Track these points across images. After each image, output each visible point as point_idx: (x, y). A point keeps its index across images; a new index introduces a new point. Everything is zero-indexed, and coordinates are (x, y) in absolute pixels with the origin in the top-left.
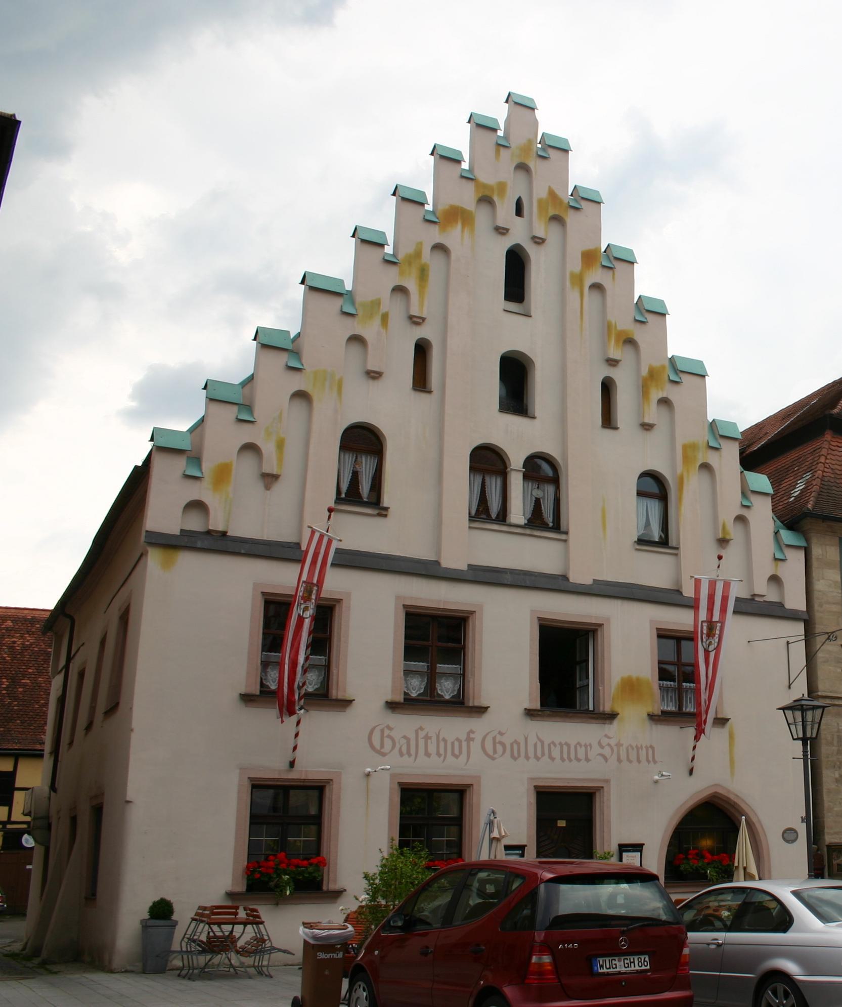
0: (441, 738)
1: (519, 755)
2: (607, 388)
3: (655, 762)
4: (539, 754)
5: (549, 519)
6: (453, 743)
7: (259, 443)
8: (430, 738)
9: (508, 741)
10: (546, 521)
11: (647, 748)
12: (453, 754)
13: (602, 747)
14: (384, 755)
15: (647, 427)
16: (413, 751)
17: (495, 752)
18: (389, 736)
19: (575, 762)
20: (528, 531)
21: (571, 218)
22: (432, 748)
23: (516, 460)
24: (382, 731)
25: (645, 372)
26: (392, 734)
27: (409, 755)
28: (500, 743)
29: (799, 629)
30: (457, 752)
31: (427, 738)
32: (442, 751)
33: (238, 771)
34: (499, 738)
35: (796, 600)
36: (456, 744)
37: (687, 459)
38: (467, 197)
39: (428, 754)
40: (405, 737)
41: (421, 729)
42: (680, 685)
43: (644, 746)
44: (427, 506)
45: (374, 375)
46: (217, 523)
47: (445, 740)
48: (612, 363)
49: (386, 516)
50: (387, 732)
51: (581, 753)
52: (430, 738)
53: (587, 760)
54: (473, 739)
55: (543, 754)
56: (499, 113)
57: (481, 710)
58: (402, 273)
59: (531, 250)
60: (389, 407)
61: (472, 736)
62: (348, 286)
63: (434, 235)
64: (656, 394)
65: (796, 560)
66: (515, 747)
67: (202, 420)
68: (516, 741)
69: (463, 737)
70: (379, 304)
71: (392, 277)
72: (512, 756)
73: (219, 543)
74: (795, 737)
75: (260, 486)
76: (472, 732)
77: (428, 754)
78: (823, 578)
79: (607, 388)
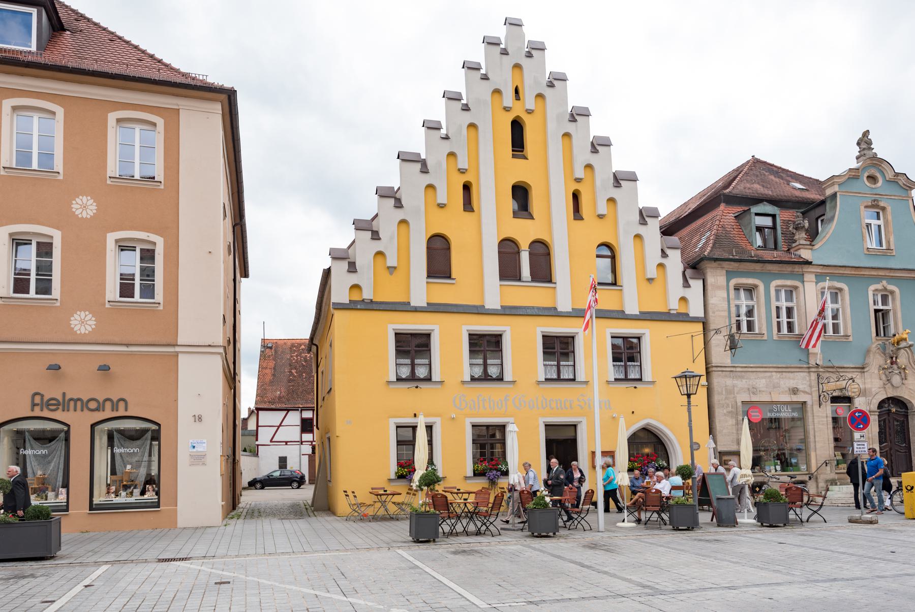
2: (576, 196)
10: (543, 272)
23: (524, 245)
29: (700, 327)
35: (696, 310)
44: (478, 275)
45: (441, 206)
46: (367, 294)
48: (578, 180)
56: (500, 32)
60: (454, 225)
62: (423, 157)
65: (697, 285)
67: (354, 241)
71: (446, 147)
73: (371, 306)
74: (201, 125)
79: (576, 196)
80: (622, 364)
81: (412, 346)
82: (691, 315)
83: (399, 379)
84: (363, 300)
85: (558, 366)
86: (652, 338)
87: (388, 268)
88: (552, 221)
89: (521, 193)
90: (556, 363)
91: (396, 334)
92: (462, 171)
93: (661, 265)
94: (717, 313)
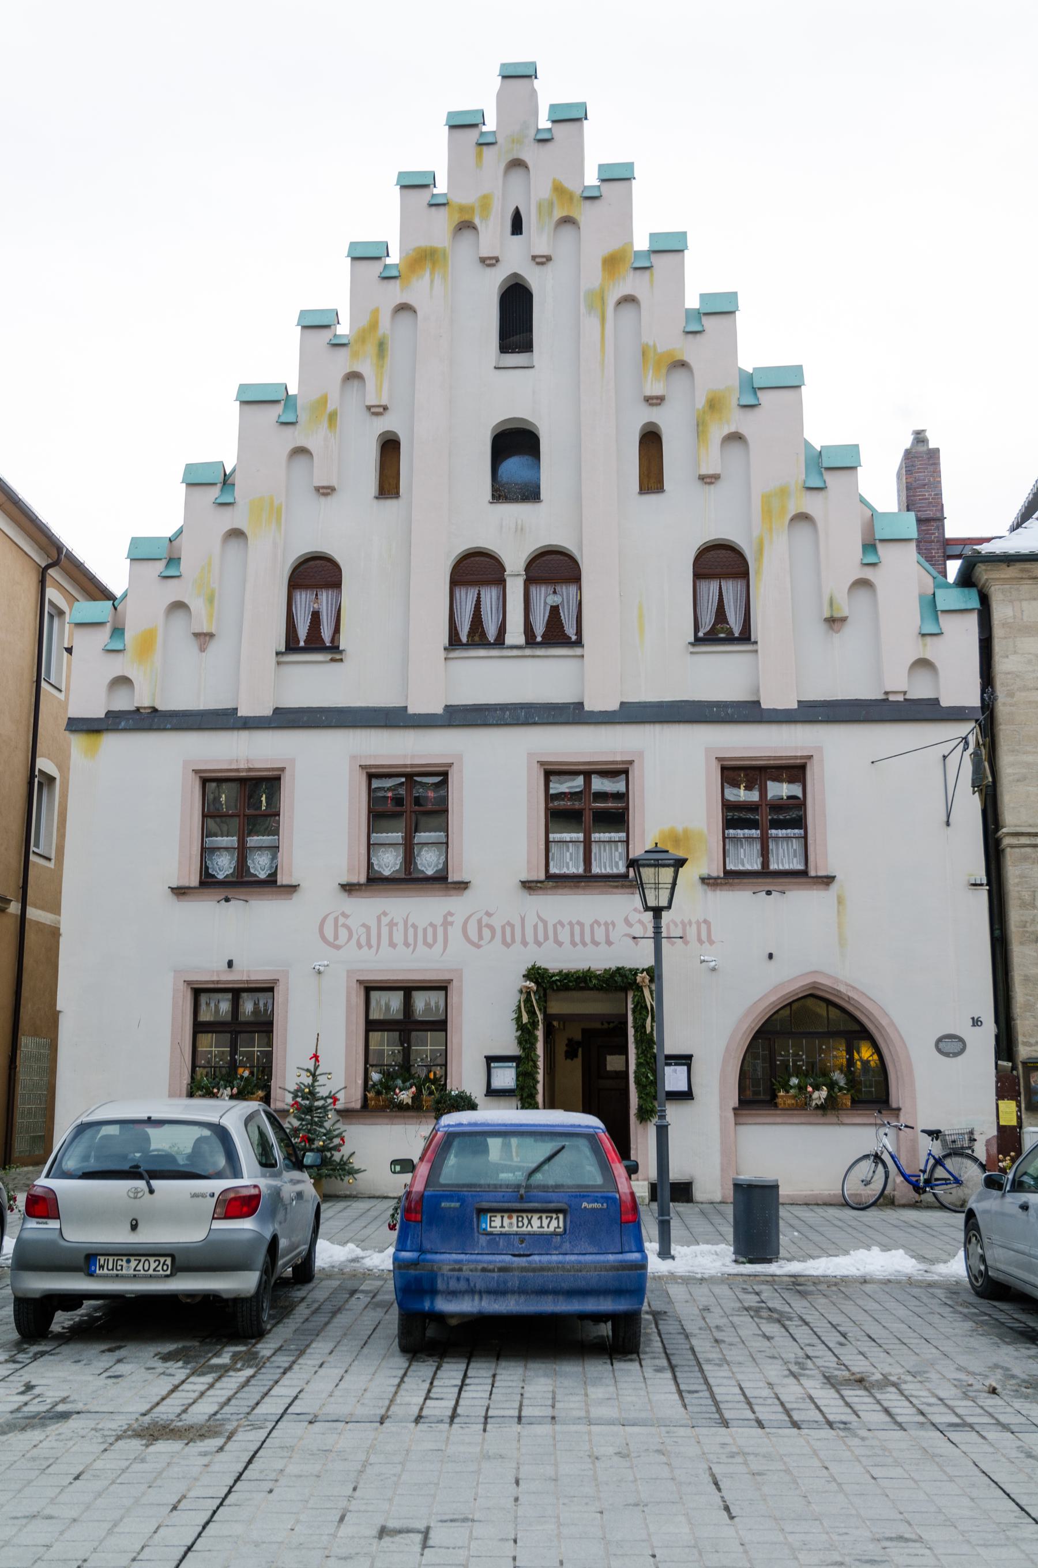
0: (410, 923)
1: (513, 941)
2: (651, 440)
3: (711, 942)
4: (541, 938)
5: (571, 631)
6: (425, 930)
7: (186, 601)
8: (396, 924)
9: (497, 922)
10: (557, 634)
11: (698, 923)
12: (425, 943)
13: (630, 925)
14: (338, 948)
15: (709, 480)
16: (374, 942)
17: (481, 938)
18: (344, 925)
19: (591, 946)
20: (528, 652)
21: (586, 214)
22: (398, 937)
23: (515, 562)
24: (336, 920)
25: (701, 402)
26: (349, 922)
27: (370, 947)
28: (488, 926)
30: (430, 940)
31: (392, 924)
32: (411, 940)
33: (172, 974)
34: (485, 920)
35: (961, 688)
36: (430, 930)
37: (768, 512)
38: (438, 230)
39: (392, 945)
40: (364, 925)
41: (385, 914)
42: (242, 842)
43: (694, 920)
45: (326, 491)
46: (142, 697)
47: (415, 927)
48: (655, 401)
49: (341, 660)
50: (342, 920)
51: (600, 934)
52: (396, 924)
53: (609, 943)
54: (451, 924)
55: (546, 938)
56: (483, 96)
57: (463, 886)
58: (355, 355)
59: (536, 280)
60: (348, 526)
61: (450, 919)
63: (395, 294)
64: (717, 432)
66: (508, 930)
68: (509, 923)
69: (438, 921)
70: (326, 402)
71: (341, 363)
72: (504, 942)
75: (193, 645)
76: (450, 914)
77: (392, 945)
78: (1015, 652)
80: (755, 833)
81: (243, 806)
82: (945, 703)
83: (208, 881)
84: (138, 709)
85: (587, 844)
86: (841, 761)
87: (197, 635)
88: (583, 499)
89: (515, 443)
90: (580, 836)
91: (724, 769)
92: (378, 411)
93: (863, 584)
94: (1021, 696)
